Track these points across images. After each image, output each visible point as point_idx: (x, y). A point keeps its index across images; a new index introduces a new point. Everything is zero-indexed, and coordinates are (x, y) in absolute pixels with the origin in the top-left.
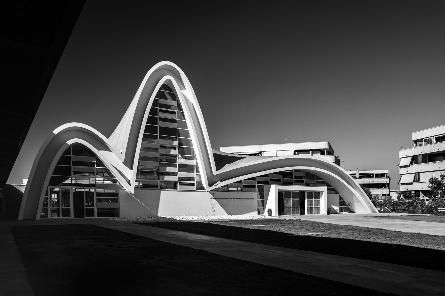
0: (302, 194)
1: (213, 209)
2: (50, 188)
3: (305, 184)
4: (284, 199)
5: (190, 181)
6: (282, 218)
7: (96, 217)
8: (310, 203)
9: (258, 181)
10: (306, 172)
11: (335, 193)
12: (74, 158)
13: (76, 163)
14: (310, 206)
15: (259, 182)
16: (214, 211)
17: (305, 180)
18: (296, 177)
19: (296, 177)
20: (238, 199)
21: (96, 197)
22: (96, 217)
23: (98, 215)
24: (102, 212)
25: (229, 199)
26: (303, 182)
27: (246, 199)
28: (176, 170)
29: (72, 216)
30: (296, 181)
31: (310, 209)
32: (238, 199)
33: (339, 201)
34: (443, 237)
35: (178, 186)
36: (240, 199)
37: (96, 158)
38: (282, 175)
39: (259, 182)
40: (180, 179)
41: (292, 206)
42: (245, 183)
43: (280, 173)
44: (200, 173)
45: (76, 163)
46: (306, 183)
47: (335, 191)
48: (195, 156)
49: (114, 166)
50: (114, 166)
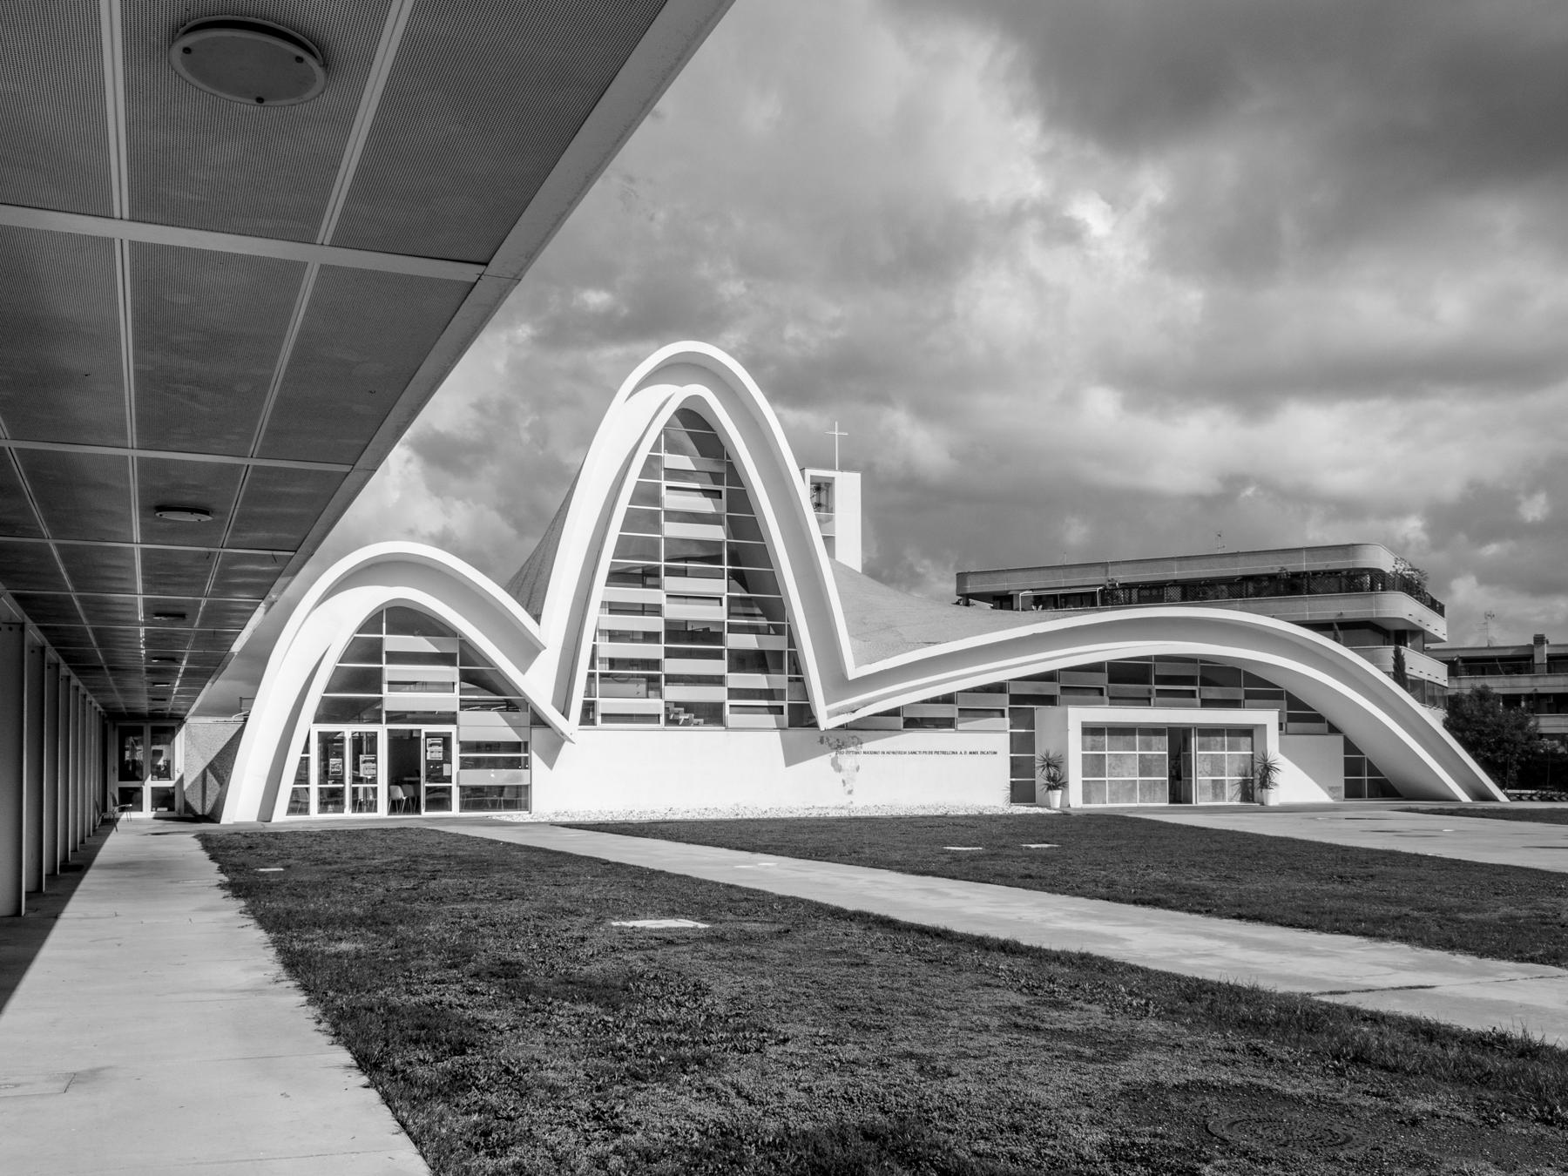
0: (1179, 738)
1: (847, 785)
2: (351, 730)
3: (1198, 701)
4: (1198, 753)
5: (774, 700)
6: (176, 809)
7: (455, 811)
8: (1209, 766)
9: (1011, 696)
10: (1202, 661)
11: (1327, 731)
12: (394, 642)
13: (395, 657)
14: (1210, 775)
15: (1015, 699)
16: (850, 792)
17: (1200, 689)
18: (1161, 680)
19: (1161, 680)
20: (937, 753)
21: (459, 755)
22: (455, 811)
23: (465, 806)
24: (476, 798)
25: (905, 753)
26: (1192, 694)
27: (965, 753)
28: (718, 667)
29: (383, 810)
30: (1160, 693)
31: (1209, 784)
32: (937, 753)
33: (1345, 758)
34: (1562, 876)
35: (662, 712)
36: (944, 753)
37: (460, 640)
38: (1107, 674)
39: (1015, 699)
40: (734, 693)
41: (1368, 775)
42: (195, 663)
43: (1095, 668)
44: (802, 674)
45: (395, 657)
46: (1202, 700)
47: (1326, 724)
48: (786, 623)
49: (326, 652)
50: (326, 652)
